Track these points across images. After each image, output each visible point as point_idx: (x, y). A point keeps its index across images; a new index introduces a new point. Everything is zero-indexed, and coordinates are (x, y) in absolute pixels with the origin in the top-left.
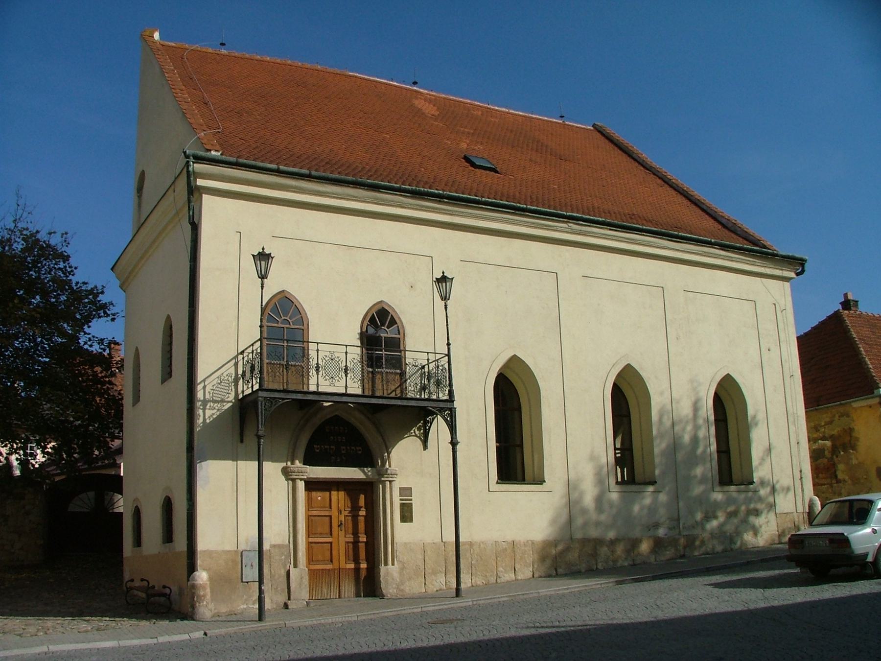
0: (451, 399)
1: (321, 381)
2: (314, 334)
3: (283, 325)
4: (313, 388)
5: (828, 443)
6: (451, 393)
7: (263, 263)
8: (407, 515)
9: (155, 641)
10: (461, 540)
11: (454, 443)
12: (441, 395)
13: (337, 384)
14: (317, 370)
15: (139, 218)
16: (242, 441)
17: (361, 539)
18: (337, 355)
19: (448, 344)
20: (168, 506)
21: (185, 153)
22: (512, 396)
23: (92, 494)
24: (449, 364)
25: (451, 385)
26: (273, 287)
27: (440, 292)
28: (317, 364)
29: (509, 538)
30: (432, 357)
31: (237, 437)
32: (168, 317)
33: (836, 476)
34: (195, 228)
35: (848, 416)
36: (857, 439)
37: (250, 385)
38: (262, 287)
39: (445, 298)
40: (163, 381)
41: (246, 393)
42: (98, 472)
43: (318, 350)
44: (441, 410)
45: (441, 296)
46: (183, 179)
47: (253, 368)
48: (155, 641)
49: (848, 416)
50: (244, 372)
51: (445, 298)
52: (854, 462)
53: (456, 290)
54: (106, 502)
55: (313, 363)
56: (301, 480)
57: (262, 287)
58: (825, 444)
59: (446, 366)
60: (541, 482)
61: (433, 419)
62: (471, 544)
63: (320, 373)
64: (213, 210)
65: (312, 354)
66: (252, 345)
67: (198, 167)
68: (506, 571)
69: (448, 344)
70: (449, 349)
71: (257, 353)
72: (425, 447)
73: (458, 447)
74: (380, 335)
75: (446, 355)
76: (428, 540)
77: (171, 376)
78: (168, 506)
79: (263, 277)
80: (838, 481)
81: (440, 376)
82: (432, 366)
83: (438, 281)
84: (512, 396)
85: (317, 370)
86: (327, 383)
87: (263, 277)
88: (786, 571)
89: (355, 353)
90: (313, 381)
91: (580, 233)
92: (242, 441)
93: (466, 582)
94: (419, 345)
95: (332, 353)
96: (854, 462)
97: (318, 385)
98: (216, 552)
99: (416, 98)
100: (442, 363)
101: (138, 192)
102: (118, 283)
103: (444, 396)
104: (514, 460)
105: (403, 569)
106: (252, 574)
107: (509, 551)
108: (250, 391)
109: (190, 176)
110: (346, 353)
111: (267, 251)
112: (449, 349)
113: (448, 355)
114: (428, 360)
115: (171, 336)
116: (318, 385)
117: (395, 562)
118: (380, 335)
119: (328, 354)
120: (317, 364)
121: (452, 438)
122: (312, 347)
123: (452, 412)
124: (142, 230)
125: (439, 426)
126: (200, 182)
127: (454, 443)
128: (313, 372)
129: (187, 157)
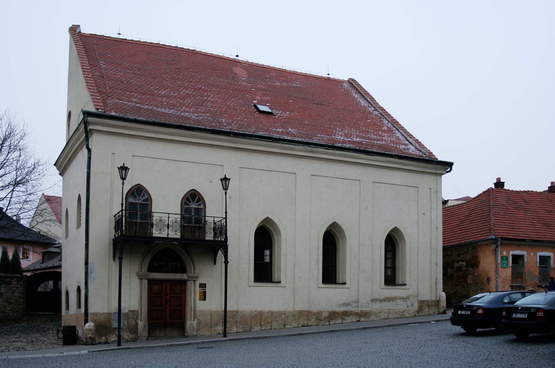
5: (464, 263)
8: (203, 297)
10: (228, 309)
13: (163, 233)
18: (163, 218)
19: (226, 213)
20: (79, 289)
23: (39, 289)
25: (226, 234)
29: (259, 309)
33: (466, 281)
35: (476, 249)
36: (479, 262)
39: (226, 189)
49: (476, 249)
51: (226, 189)
52: (476, 274)
56: (146, 279)
58: (463, 264)
67: (90, 119)
68: (256, 326)
69: (226, 213)
70: (226, 215)
72: (215, 264)
73: (228, 264)
76: (214, 309)
78: (79, 289)
79: (123, 179)
80: (468, 284)
81: (221, 230)
83: (222, 180)
84: (265, 236)
86: (173, 233)
87: (123, 179)
88: (487, 329)
91: (311, 152)
94: (213, 212)
95: (161, 217)
96: (476, 274)
97: (168, 234)
98: (99, 313)
99: (237, 66)
102: (58, 172)
104: (264, 272)
105: (198, 324)
106: (115, 325)
107: (258, 316)
111: (126, 166)
112: (226, 215)
113: (226, 218)
116: (168, 234)
117: (196, 320)
123: (226, 247)
125: (220, 254)
126: (91, 127)
127: (226, 262)
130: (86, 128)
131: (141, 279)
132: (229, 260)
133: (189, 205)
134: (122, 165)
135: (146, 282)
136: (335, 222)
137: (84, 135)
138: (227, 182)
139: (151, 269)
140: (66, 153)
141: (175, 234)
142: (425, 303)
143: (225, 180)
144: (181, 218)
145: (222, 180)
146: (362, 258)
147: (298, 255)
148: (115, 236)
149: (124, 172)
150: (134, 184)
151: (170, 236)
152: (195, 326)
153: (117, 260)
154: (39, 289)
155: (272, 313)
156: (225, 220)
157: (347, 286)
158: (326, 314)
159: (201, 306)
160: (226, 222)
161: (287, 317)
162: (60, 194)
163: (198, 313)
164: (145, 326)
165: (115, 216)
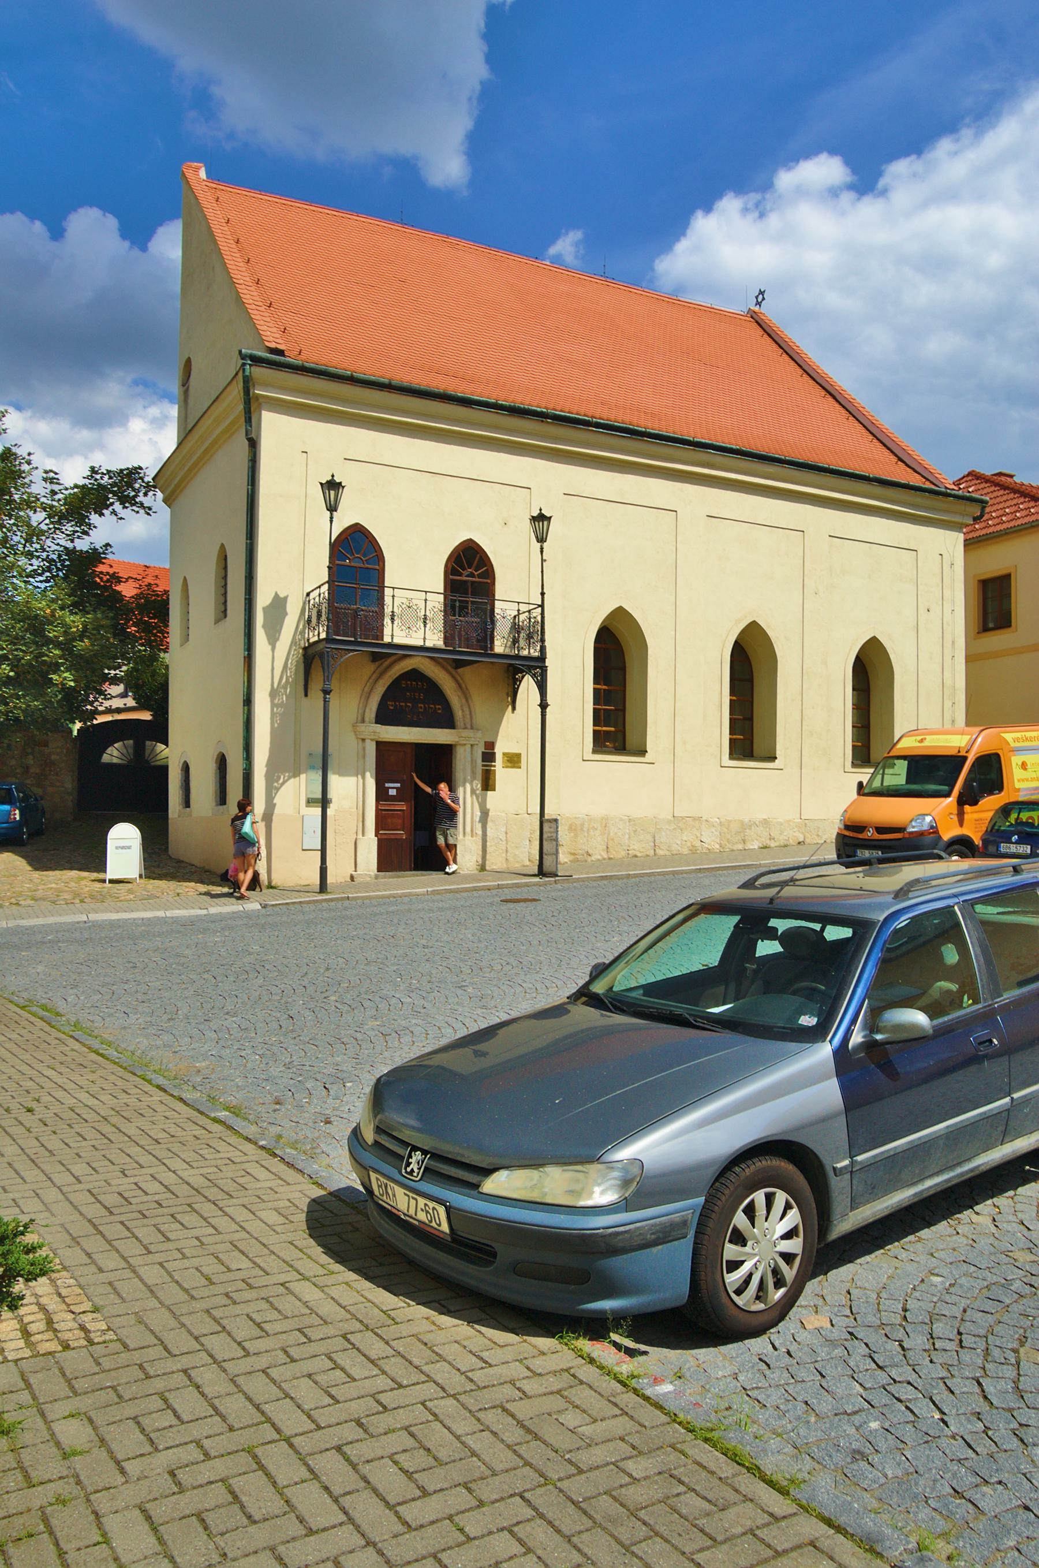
0: (542, 658)
2: (391, 578)
3: (356, 558)
4: (387, 639)
6: (543, 649)
7: (332, 493)
9: (204, 912)
11: (544, 706)
12: (532, 651)
13: (414, 635)
14: (393, 620)
15: (185, 428)
16: (306, 695)
17: (829, 928)
18: (415, 602)
19: (543, 594)
20: (222, 762)
21: (240, 352)
22: (616, 652)
23: (106, 758)
24: (543, 618)
25: (543, 640)
26: (344, 520)
27: (535, 532)
30: (524, 608)
32: (222, 545)
34: (253, 444)
37: (316, 633)
38: (331, 521)
39: (541, 539)
40: (217, 621)
41: (311, 641)
42: (850, 902)
44: (529, 670)
45: (537, 537)
46: (238, 387)
47: (319, 616)
48: (204, 912)
50: (310, 617)
51: (541, 539)
53: (555, 529)
54: (147, 753)
55: (388, 610)
57: (331, 521)
59: (539, 618)
60: (643, 752)
61: (523, 677)
63: (396, 623)
64: (274, 427)
65: (388, 600)
66: (319, 587)
69: (543, 594)
71: (324, 598)
73: (548, 710)
74: (469, 573)
77: (225, 617)
78: (222, 762)
79: (332, 508)
82: (522, 617)
83: (534, 519)
84: (616, 652)
85: (393, 620)
86: (403, 634)
87: (332, 508)
89: (437, 601)
90: (387, 631)
92: (306, 695)
94: (511, 594)
97: (425, 639)
100: (535, 615)
101: (183, 385)
103: (535, 653)
104: (616, 726)
108: (316, 639)
109: (248, 383)
110: (426, 600)
113: (542, 606)
115: (225, 568)
116: (425, 639)
118: (469, 573)
121: (542, 700)
122: (388, 592)
123: (544, 670)
124: (189, 438)
125: (528, 686)
127: (544, 706)
128: (387, 621)
129: (243, 357)
130: (247, 391)
132: (550, 699)
133: (461, 575)
136: (754, 623)
137: (241, 407)
138: (545, 523)
139: (383, 718)
141: (435, 639)
143: (541, 519)
144: (445, 605)
146: (812, 703)
147: (685, 692)
150: (347, 525)
153: (316, 699)
154: (106, 758)
157: (648, 757)
160: (543, 614)
162: (167, 566)
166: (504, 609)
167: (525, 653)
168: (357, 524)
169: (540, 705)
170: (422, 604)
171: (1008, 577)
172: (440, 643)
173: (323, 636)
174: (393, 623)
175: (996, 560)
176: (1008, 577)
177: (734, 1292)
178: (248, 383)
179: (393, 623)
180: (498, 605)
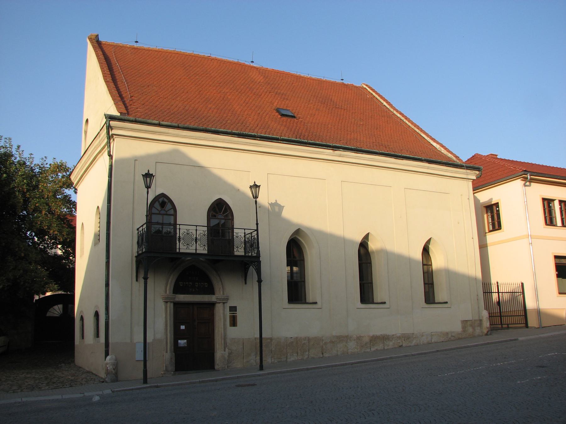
1: (198, 247)
6: (258, 252)
8: (234, 322)
9: (82, 395)
16: (246, 283)
18: (191, 231)
19: (257, 224)
20: (97, 314)
23: (61, 306)
25: (258, 248)
28: (196, 238)
31: (244, 282)
43: (196, 230)
46: (105, 131)
48: (82, 395)
56: (171, 302)
59: (256, 236)
62: (271, 339)
66: (142, 226)
67: (113, 123)
69: (257, 224)
75: (256, 230)
78: (97, 314)
79: (148, 187)
81: (252, 243)
83: (251, 187)
86: (185, 247)
87: (148, 187)
93: (268, 360)
94: (242, 224)
95: (188, 230)
97: (196, 250)
111: (151, 173)
113: (257, 230)
114: (245, 233)
116: (196, 250)
117: (227, 350)
119: (185, 231)
120: (196, 238)
122: (178, 226)
123: (259, 262)
126: (114, 132)
130: (108, 133)
131: (167, 302)
134: (147, 172)
135: (172, 304)
137: (106, 140)
140: (83, 162)
141: (202, 250)
142: (469, 323)
145: (251, 187)
148: (138, 252)
149: (148, 179)
151: (198, 252)
152: (226, 356)
155: (309, 339)
156: (256, 232)
158: (367, 339)
159: (232, 332)
160: (257, 234)
161: (326, 343)
163: (228, 341)
164: (171, 358)
165: (138, 229)
166: (239, 233)
167: (250, 254)
168: (163, 194)
169: (258, 281)
170: (194, 232)
171: (498, 203)
172: (206, 252)
173: (144, 250)
174: (196, 243)
175: (485, 196)
176: (498, 203)
177: (230, 307)
178: (109, 128)
179: (196, 243)
180: (235, 231)
